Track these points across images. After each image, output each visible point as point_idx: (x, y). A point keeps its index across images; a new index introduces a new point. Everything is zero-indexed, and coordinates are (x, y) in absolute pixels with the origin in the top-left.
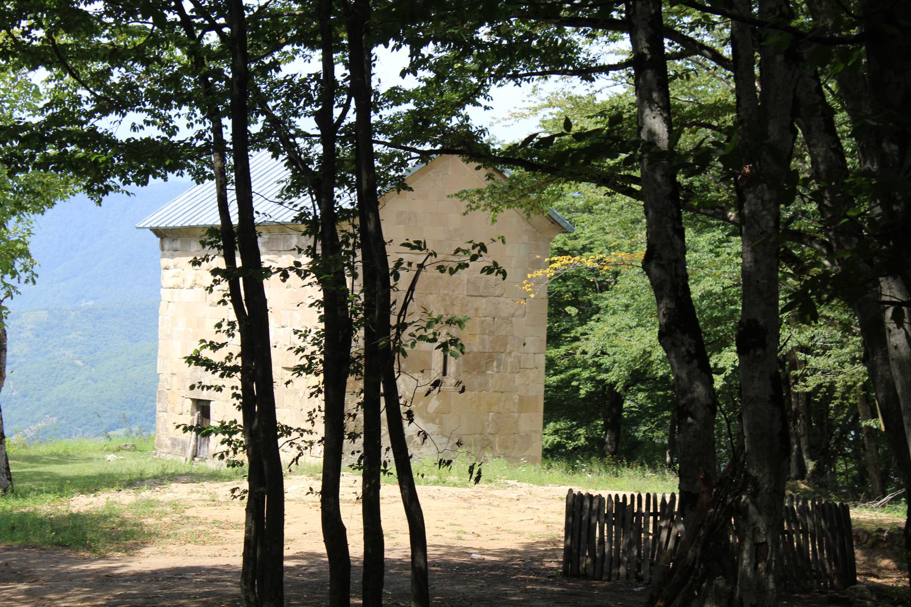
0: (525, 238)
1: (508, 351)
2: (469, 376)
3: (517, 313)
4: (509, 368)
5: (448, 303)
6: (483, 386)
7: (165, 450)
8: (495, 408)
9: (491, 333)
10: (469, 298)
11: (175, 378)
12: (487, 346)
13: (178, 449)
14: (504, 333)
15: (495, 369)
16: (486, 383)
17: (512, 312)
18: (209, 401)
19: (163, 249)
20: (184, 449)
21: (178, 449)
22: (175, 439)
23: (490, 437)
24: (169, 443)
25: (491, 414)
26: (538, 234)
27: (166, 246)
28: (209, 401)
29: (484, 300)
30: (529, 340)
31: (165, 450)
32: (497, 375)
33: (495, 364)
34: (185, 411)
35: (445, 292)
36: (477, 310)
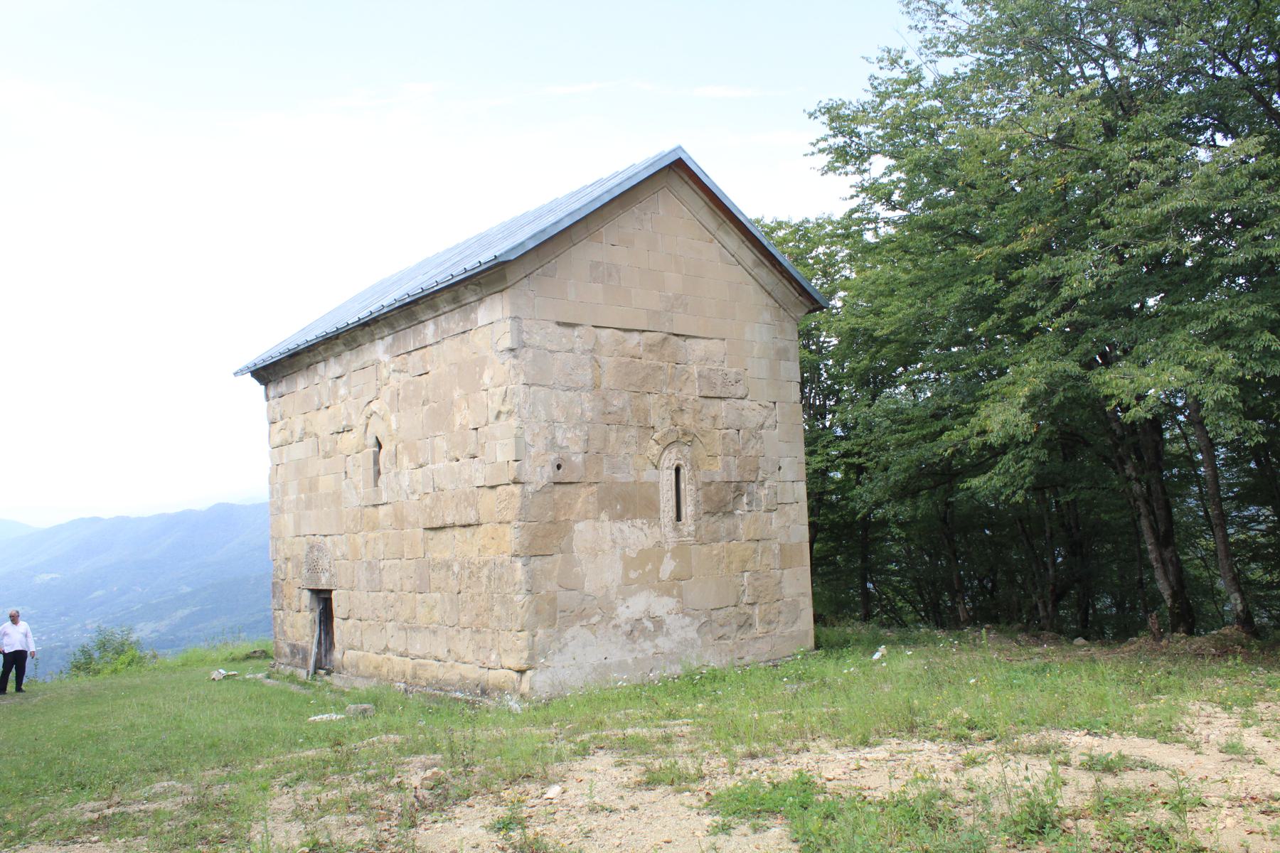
0: (767, 316)
1: (760, 479)
2: (713, 519)
3: (767, 424)
4: (764, 504)
5: (675, 407)
6: (732, 536)
7: (284, 660)
8: (749, 566)
9: (737, 454)
10: (703, 401)
11: (290, 565)
12: (734, 473)
13: (298, 659)
14: (753, 453)
15: (746, 508)
16: (736, 527)
17: (761, 421)
18: (330, 591)
19: (267, 398)
20: (305, 659)
21: (298, 659)
22: (294, 646)
23: (748, 610)
24: (287, 650)
25: (746, 574)
26: (782, 311)
27: (271, 394)
28: (330, 591)
29: (723, 403)
30: (785, 463)
31: (284, 660)
32: (749, 515)
33: (745, 499)
34: (303, 607)
35: (669, 391)
36: (715, 418)
